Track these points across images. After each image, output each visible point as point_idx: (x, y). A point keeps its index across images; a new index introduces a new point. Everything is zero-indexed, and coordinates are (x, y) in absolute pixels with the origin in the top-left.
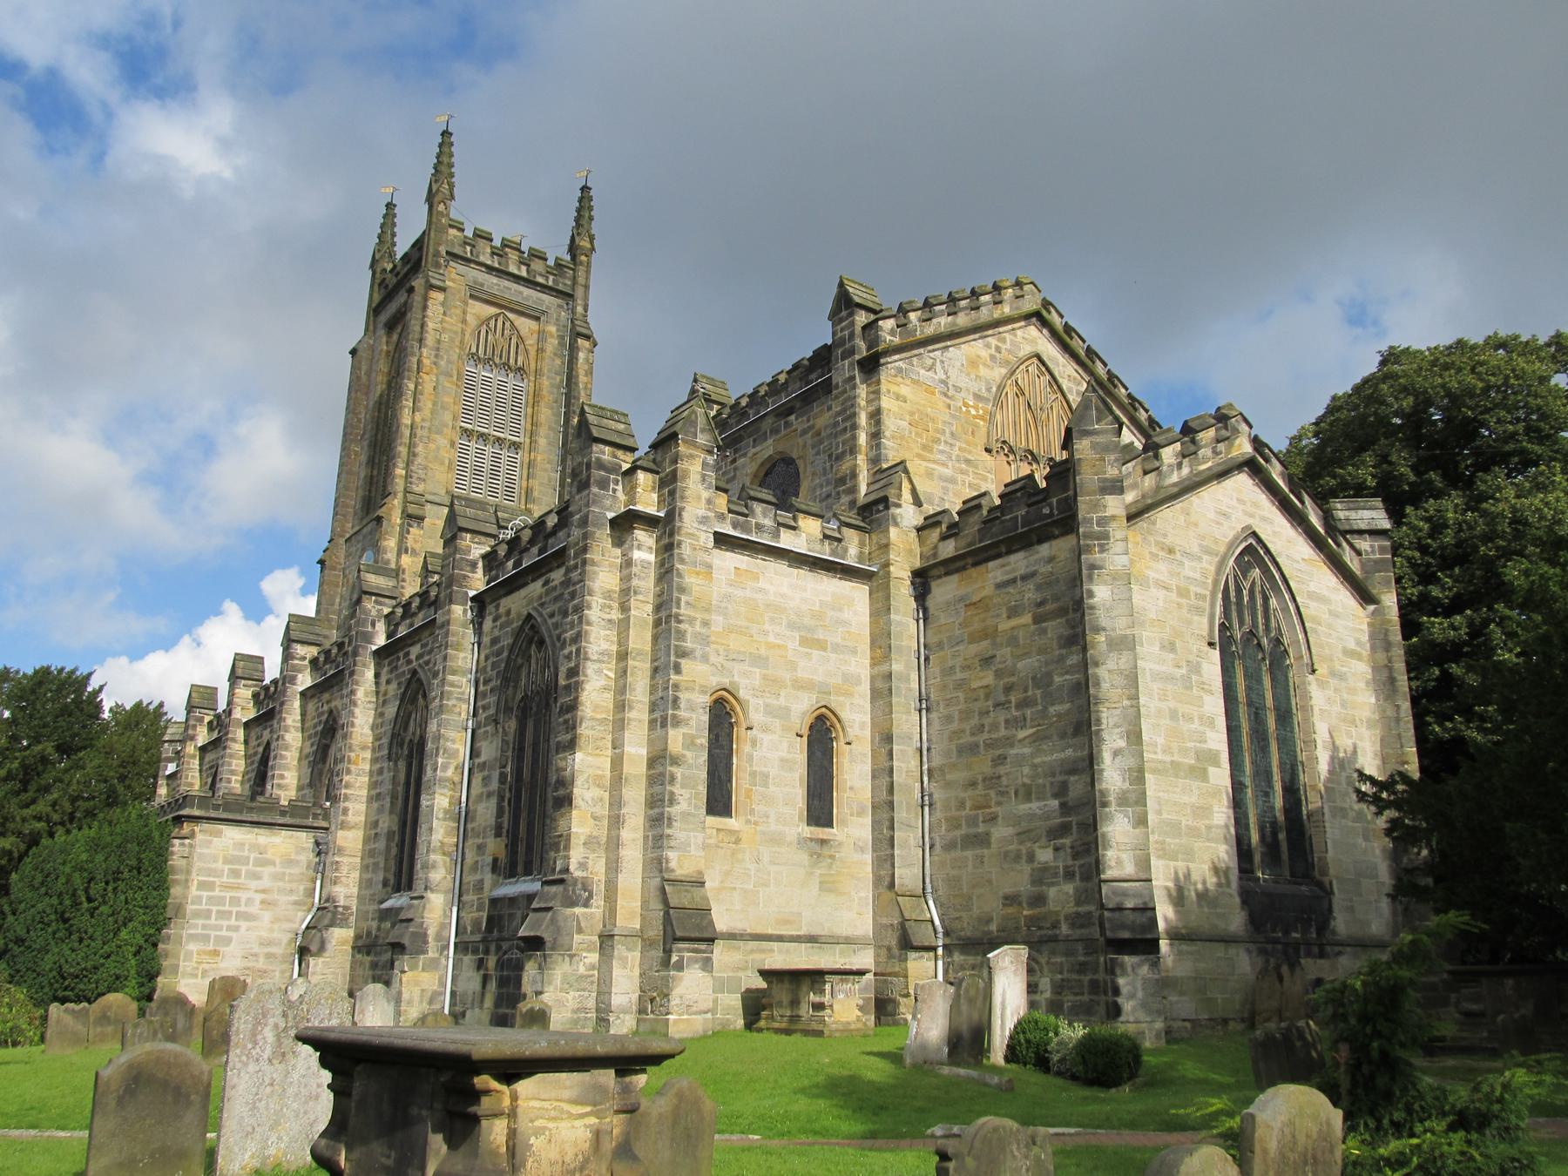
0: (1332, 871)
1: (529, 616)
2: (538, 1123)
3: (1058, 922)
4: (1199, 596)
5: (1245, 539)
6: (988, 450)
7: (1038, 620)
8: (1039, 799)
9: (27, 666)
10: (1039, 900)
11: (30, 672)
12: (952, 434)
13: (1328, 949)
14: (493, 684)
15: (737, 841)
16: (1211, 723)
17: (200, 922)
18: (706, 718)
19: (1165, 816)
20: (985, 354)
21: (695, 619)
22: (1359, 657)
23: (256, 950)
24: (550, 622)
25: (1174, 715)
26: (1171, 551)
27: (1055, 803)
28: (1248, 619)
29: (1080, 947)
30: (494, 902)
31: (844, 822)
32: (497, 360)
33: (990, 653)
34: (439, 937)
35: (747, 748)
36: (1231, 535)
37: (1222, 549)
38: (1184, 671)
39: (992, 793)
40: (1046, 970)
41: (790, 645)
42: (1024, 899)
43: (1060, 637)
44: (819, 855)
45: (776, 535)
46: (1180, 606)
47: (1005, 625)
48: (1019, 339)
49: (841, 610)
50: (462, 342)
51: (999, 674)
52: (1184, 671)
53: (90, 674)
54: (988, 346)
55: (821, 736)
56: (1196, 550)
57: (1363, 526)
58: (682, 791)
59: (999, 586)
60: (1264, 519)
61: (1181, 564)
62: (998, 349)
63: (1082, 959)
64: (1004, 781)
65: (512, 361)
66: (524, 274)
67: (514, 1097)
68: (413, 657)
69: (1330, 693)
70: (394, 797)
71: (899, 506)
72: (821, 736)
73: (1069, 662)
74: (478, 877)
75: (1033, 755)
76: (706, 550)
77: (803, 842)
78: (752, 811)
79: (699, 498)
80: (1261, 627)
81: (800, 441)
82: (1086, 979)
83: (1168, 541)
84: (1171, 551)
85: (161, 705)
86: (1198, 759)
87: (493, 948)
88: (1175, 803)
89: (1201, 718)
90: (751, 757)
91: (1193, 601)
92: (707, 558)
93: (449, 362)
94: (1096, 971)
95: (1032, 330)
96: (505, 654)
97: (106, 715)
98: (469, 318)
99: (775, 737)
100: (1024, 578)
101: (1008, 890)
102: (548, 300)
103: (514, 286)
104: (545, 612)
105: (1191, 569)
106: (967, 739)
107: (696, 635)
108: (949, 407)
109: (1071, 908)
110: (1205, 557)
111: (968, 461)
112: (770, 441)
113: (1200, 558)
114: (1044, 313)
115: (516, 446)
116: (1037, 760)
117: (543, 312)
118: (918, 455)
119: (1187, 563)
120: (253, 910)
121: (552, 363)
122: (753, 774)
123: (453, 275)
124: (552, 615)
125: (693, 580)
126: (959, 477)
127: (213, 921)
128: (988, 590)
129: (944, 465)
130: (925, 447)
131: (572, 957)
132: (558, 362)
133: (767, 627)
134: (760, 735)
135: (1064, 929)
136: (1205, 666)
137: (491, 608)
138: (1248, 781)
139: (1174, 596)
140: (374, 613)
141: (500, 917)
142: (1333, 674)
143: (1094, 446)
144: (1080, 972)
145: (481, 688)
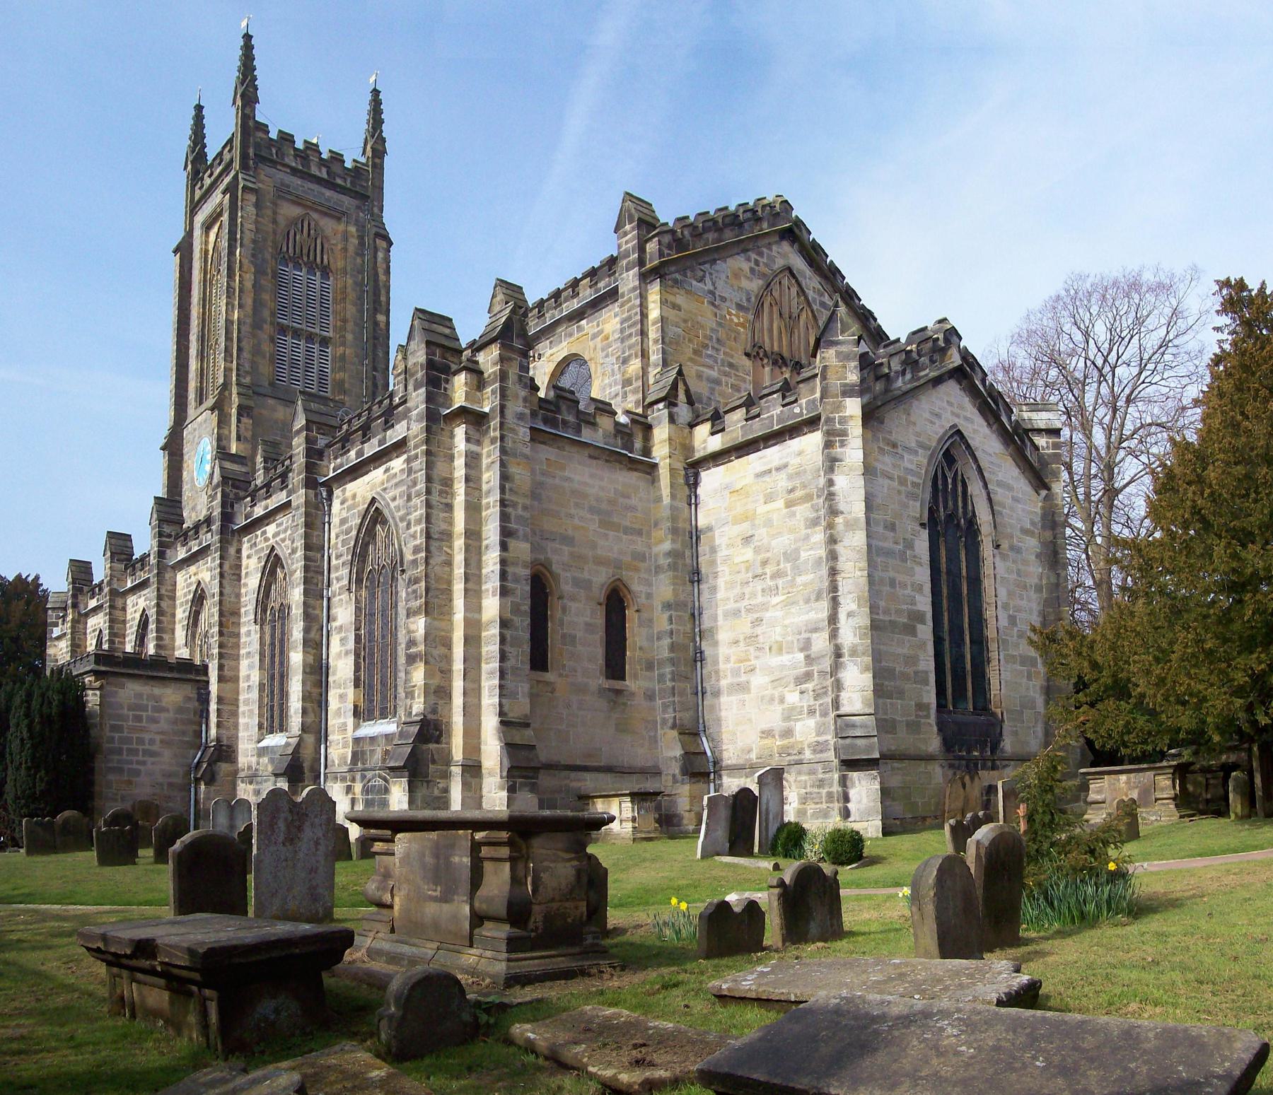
1: (373, 500)
2: (545, 864)
3: (803, 749)
4: (914, 484)
6: (747, 355)
7: (789, 504)
10: (788, 733)
12: (718, 340)
14: (344, 558)
16: (920, 589)
17: (116, 757)
19: (884, 664)
20: (746, 266)
23: (160, 779)
24: (392, 505)
26: (894, 446)
27: (801, 656)
28: (950, 503)
29: (819, 767)
30: (357, 741)
33: (750, 533)
35: (559, 614)
38: (901, 547)
39: (752, 649)
40: (793, 788)
45: (579, 432)
46: (899, 492)
48: (774, 253)
49: (628, 497)
51: (757, 550)
52: (901, 547)
54: (749, 260)
56: (913, 445)
57: (1042, 426)
58: (512, 650)
59: (758, 475)
60: (966, 419)
61: (902, 457)
63: (821, 776)
64: (761, 639)
66: (325, 176)
68: (269, 535)
69: (1009, 564)
70: (262, 655)
72: (616, 604)
73: (813, 540)
74: (342, 720)
77: (602, 692)
79: (517, 396)
80: (961, 510)
81: (591, 343)
82: (824, 792)
84: (894, 446)
85: (37, 578)
86: (909, 618)
87: (358, 776)
94: (831, 785)
95: (786, 246)
96: (354, 533)
98: (282, 221)
100: (778, 469)
102: (347, 202)
104: (388, 496)
105: (909, 461)
107: (519, 518)
109: (812, 738)
111: (731, 365)
112: (564, 344)
113: (916, 453)
114: (796, 230)
115: (325, 342)
116: (787, 622)
117: (344, 213)
118: (691, 360)
119: (906, 456)
120: (155, 748)
122: (564, 636)
124: (394, 499)
126: (724, 379)
128: (750, 479)
129: (711, 367)
131: (428, 782)
133: (573, 511)
135: (808, 755)
136: (917, 543)
138: (946, 636)
140: (232, 496)
141: (363, 753)
143: (838, 354)
144: (819, 787)
145: (334, 562)
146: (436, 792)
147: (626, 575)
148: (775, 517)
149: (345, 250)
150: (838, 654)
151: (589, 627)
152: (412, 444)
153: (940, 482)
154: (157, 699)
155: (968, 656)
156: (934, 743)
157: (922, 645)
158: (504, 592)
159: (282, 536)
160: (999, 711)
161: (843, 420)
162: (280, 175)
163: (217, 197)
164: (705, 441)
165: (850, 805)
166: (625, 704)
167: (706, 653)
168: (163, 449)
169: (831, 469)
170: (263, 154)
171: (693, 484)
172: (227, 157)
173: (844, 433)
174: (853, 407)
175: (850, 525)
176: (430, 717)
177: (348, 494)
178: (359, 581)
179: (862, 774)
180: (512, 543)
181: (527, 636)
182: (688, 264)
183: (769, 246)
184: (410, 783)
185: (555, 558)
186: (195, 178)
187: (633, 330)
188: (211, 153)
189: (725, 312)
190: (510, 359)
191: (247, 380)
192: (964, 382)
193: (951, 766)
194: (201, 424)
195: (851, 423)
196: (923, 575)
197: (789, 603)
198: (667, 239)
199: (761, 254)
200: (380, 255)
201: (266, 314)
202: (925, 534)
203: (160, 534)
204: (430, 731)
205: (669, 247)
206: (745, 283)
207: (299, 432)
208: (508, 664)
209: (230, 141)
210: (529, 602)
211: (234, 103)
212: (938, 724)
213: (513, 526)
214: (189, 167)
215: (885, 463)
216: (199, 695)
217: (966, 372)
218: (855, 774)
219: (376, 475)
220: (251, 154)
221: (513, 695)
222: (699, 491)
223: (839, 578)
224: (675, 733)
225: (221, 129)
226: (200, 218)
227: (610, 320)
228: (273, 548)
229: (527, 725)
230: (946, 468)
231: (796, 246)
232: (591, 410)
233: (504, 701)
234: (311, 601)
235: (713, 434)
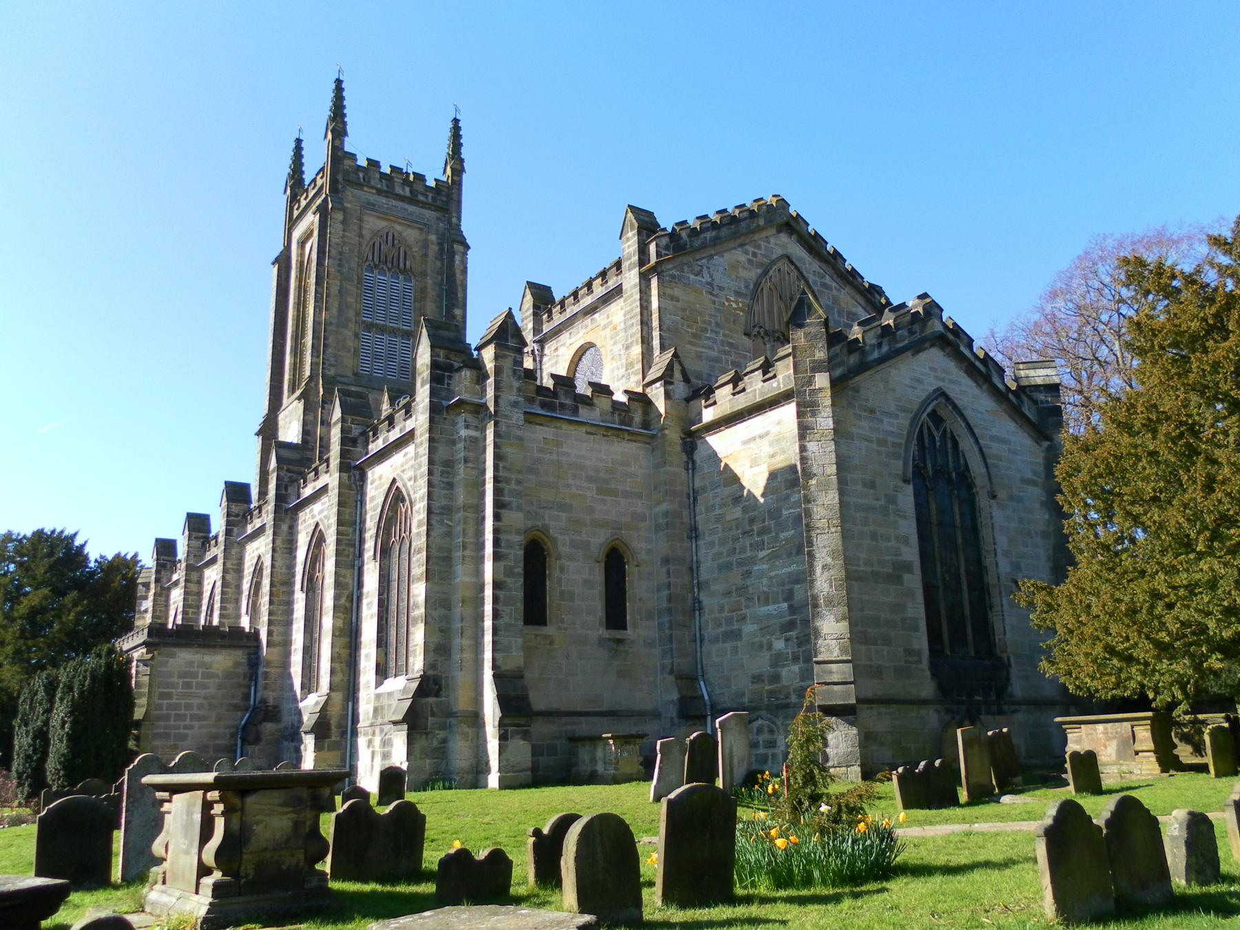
0: (1009, 650)
1: (394, 481)
4: (894, 445)
5: (936, 398)
8: (774, 603)
9: (25, 529)
10: (775, 678)
11: (29, 534)
12: (717, 324)
13: (1006, 707)
16: (906, 541)
18: (521, 552)
19: (866, 612)
20: (743, 258)
21: (510, 479)
22: (1034, 483)
25: (874, 536)
26: (872, 411)
30: (378, 696)
31: (635, 626)
34: (339, 726)
35: (557, 574)
36: (924, 395)
37: (916, 407)
38: (882, 503)
41: (589, 494)
42: (766, 678)
43: (786, 481)
44: (616, 651)
45: (575, 411)
46: (879, 453)
49: (628, 465)
50: (359, 253)
52: (882, 503)
53: (75, 534)
54: (746, 253)
55: (615, 564)
56: (893, 409)
59: (745, 442)
60: (951, 382)
61: (882, 421)
62: (755, 255)
64: (750, 590)
65: (402, 265)
67: (243, 803)
72: (615, 564)
75: (770, 570)
76: (518, 427)
77: (602, 642)
78: (562, 621)
79: (511, 387)
83: (870, 404)
85: (136, 555)
87: (378, 731)
89: (897, 537)
90: (560, 580)
92: (519, 433)
93: (350, 268)
95: (783, 237)
97: (92, 565)
98: (365, 233)
100: (761, 437)
101: (756, 671)
102: (428, 214)
103: (400, 204)
104: (406, 477)
106: (724, 559)
108: (714, 302)
110: (901, 414)
111: (730, 345)
113: (897, 416)
118: (690, 343)
119: (886, 420)
121: (433, 264)
122: (562, 593)
125: (508, 450)
130: (695, 336)
131: (427, 734)
133: (570, 481)
134: (567, 563)
136: (900, 498)
140: (286, 479)
141: (382, 708)
142: (1011, 498)
149: (425, 255)
151: (587, 583)
152: (417, 433)
153: (926, 441)
154: (207, 666)
155: (966, 604)
156: (928, 689)
157: (910, 594)
158: (497, 557)
159: (325, 513)
160: (1005, 655)
162: (368, 196)
165: (828, 750)
166: (627, 652)
167: (704, 603)
168: (257, 434)
172: (319, 182)
175: (824, 487)
176: (430, 673)
177: (376, 476)
180: (505, 513)
181: (521, 595)
183: (767, 239)
185: (552, 524)
186: (294, 199)
187: (634, 321)
188: (308, 178)
189: (723, 300)
190: (505, 356)
191: (331, 372)
192: (948, 350)
193: (949, 711)
196: (909, 527)
197: (773, 557)
198: (665, 241)
200: (457, 258)
202: (909, 489)
203: (228, 515)
205: (667, 248)
206: (743, 273)
207: (336, 423)
209: (322, 169)
210: (522, 565)
211: (326, 136)
212: (931, 669)
213: (506, 499)
214: (289, 192)
215: (862, 427)
216: (249, 660)
217: (953, 340)
219: (397, 459)
224: (671, 678)
225: (316, 158)
227: (621, 313)
228: (317, 525)
230: (933, 428)
231: (794, 237)
232: (589, 393)
233: (498, 656)
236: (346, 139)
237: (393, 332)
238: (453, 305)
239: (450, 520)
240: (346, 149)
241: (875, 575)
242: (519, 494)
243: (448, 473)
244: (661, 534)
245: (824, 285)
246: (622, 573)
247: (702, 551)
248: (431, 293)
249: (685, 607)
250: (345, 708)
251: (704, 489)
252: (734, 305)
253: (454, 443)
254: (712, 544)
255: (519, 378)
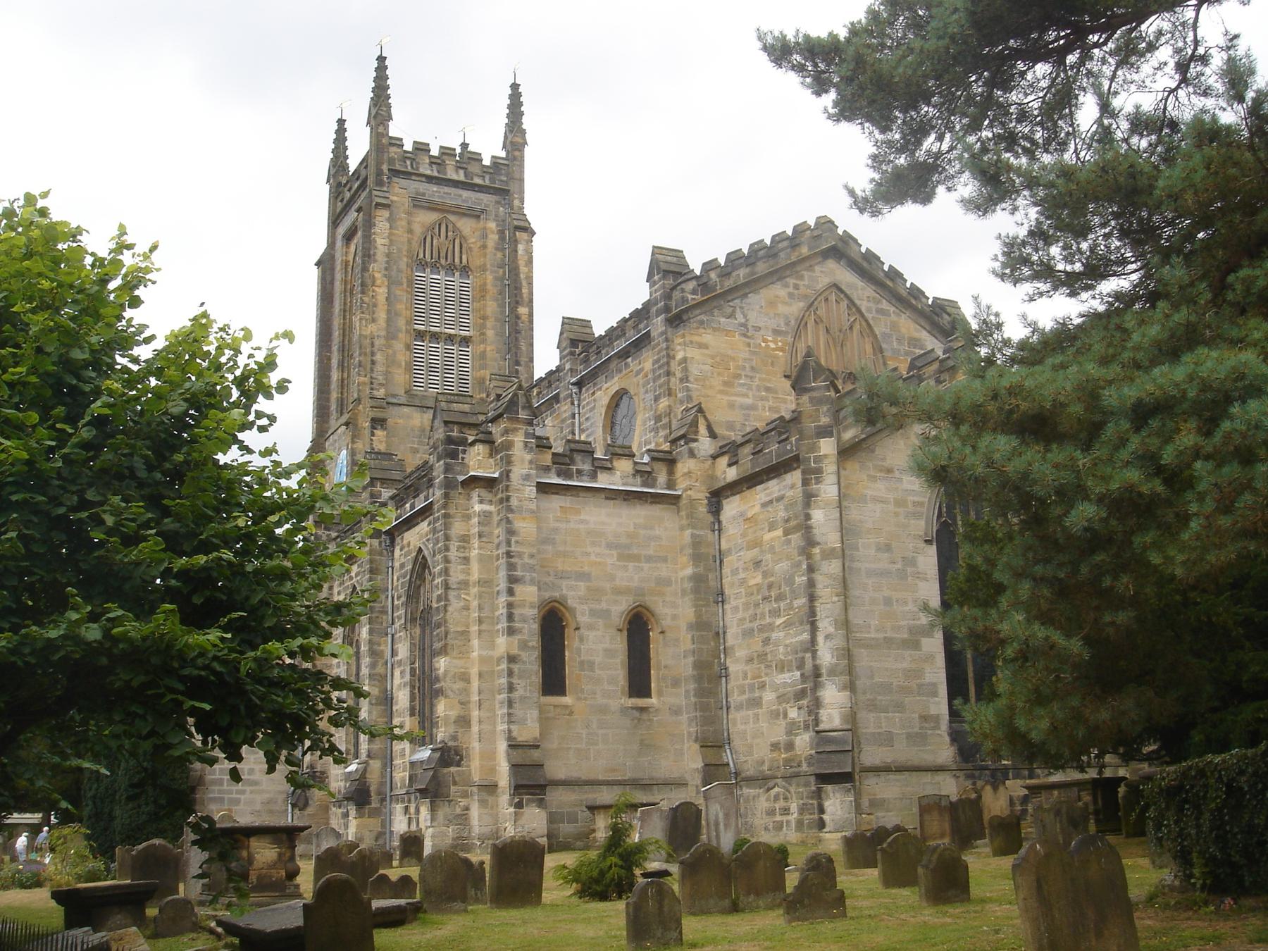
4: (915, 504)
7: (787, 533)
10: (790, 746)
12: (752, 368)
15: (571, 713)
17: (216, 788)
19: (877, 679)
26: (889, 471)
30: (412, 764)
32: (443, 261)
34: (379, 793)
35: (576, 643)
39: (763, 666)
47: (767, 537)
51: (765, 575)
52: (899, 566)
55: (638, 628)
59: (764, 505)
65: (457, 260)
71: (696, 440)
72: (638, 628)
77: (624, 711)
78: (582, 691)
79: (523, 460)
88: (886, 669)
91: (911, 508)
95: (831, 264)
99: (599, 633)
101: (774, 740)
102: (486, 199)
103: (453, 190)
106: (747, 625)
111: (768, 389)
115: (465, 341)
117: (482, 211)
118: (721, 392)
121: (492, 256)
122: (582, 663)
123: (397, 190)
127: (225, 787)
128: (757, 509)
130: (726, 384)
131: (450, 801)
132: (499, 255)
133: (589, 549)
135: (804, 767)
136: (921, 560)
137: (398, 540)
139: (891, 507)
140: (324, 538)
143: (811, 400)
145: (396, 603)
146: (458, 811)
147: (650, 601)
148: (776, 544)
149: (484, 247)
150: (817, 673)
151: (609, 653)
152: (436, 507)
156: (945, 753)
157: (930, 658)
161: (818, 459)
163: (352, 215)
164: (725, 472)
165: (824, 817)
166: (650, 720)
169: (807, 504)
170: (398, 167)
171: (716, 509)
173: (819, 471)
174: (827, 447)
178: (413, 620)
179: (836, 787)
180: (518, 589)
182: (715, 304)
184: (431, 802)
185: (570, 594)
193: (968, 777)
194: (340, 436)
195: (826, 461)
199: (802, 278)
200: (521, 248)
201: (401, 323)
202: (933, 550)
204: (449, 756)
206: (782, 309)
208: (516, 695)
212: (950, 735)
213: (519, 573)
218: (829, 787)
220: (386, 171)
221: (523, 722)
222: (722, 518)
223: (817, 604)
225: (358, 148)
226: (341, 230)
229: (537, 747)
233: (513, 727)
234: (376, 639)
235: (730, 465)
236: (390, 123)
237: (450, 339)
238: (517, 303)
239: (468, 594)
240: (391, 134)
241: (888, 641)
242: (532, 568)
243: (464, 547)
244: (686, 599)
245: (881, 311)
246: (646, 642)
247: (729, 616)
248: (492, 289)
249: (710, 674)
250: (383, 775)
251: (729, 551)
252: (772, 346)
253: (468, 517)
254: (736, 609)
255: (531, 450)
